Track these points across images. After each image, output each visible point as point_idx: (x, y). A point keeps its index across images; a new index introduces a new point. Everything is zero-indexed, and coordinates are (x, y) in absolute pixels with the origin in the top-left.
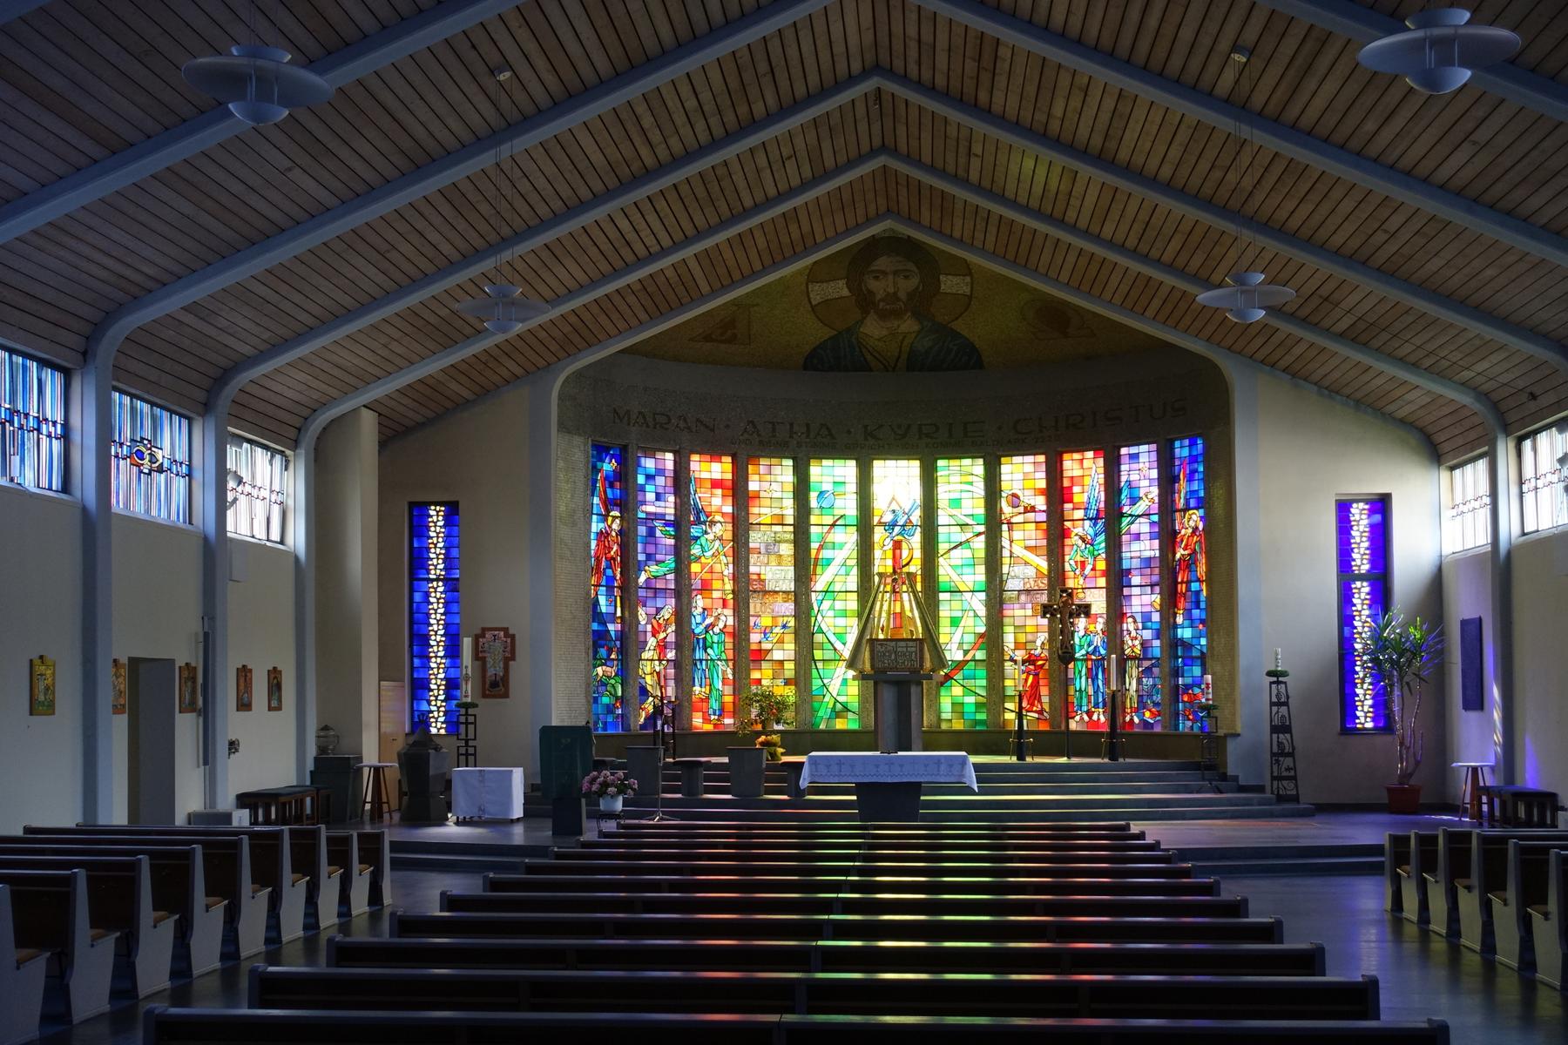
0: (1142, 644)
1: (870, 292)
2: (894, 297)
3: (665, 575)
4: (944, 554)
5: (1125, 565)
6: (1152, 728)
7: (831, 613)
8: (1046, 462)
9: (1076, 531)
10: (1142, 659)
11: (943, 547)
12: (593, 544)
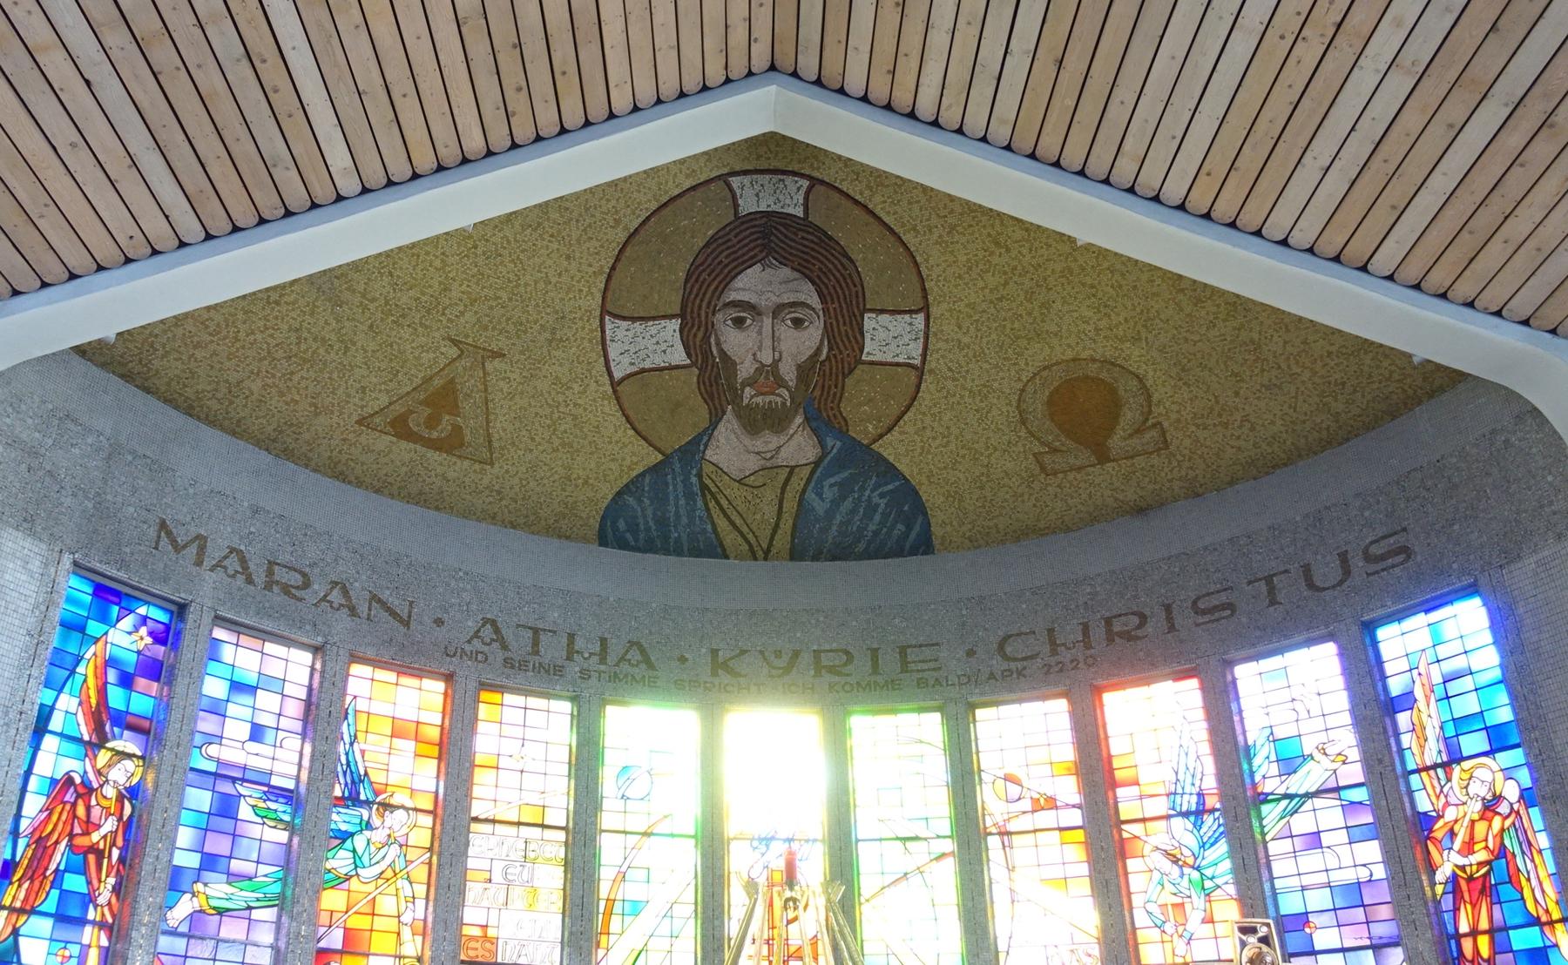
1: (729, 363)
2: (769, 374)
3: (250, 908)
5: (1290, 905)
9: (1154, 841)
12: (33, 805)
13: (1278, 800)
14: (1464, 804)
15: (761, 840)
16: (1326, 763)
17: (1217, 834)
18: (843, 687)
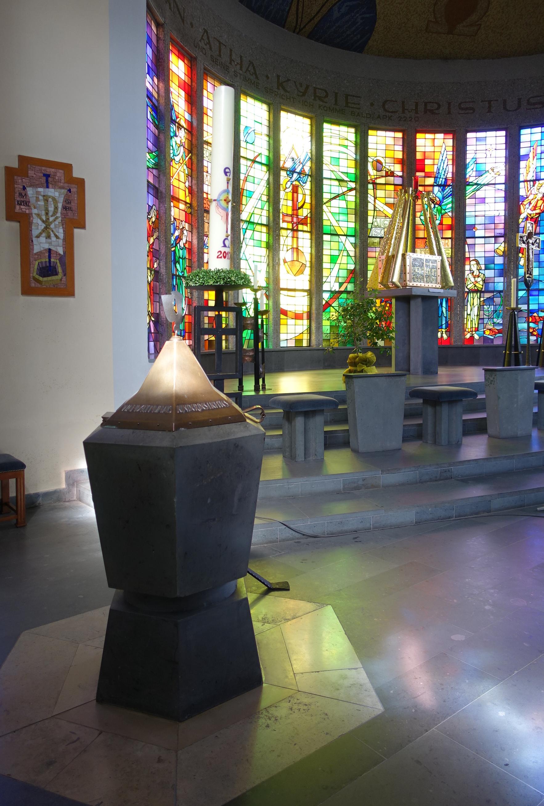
0: (484, 281)
4: (327, 202)
6: (493, 342)
7: (251, 242)
8: (403, 138)
10: (484, 292)
11: (326, 196)
13: (473, 185)
14: (537, 194)
15: (290, 171)
16: (493, 174)
17: (449, 194)
18: (324, 107)
